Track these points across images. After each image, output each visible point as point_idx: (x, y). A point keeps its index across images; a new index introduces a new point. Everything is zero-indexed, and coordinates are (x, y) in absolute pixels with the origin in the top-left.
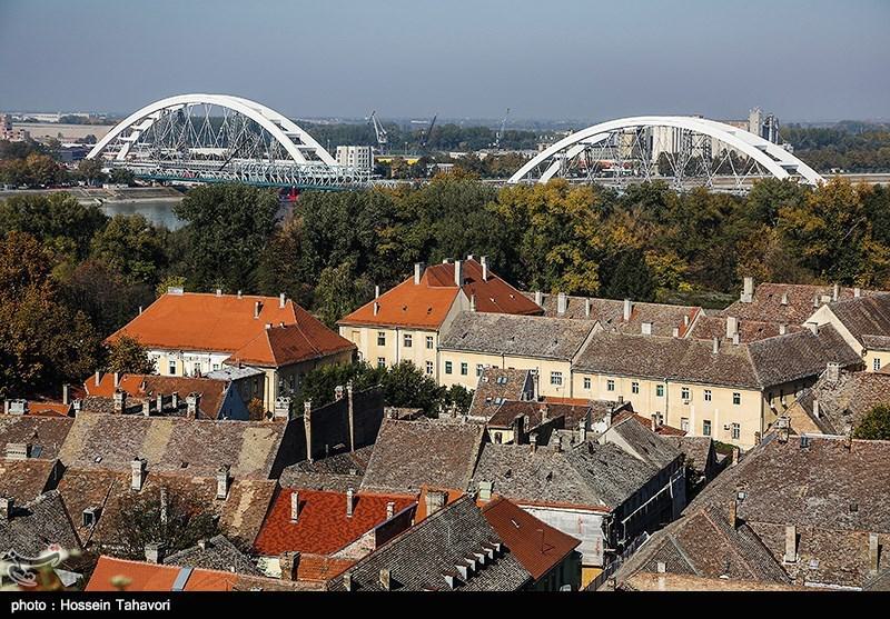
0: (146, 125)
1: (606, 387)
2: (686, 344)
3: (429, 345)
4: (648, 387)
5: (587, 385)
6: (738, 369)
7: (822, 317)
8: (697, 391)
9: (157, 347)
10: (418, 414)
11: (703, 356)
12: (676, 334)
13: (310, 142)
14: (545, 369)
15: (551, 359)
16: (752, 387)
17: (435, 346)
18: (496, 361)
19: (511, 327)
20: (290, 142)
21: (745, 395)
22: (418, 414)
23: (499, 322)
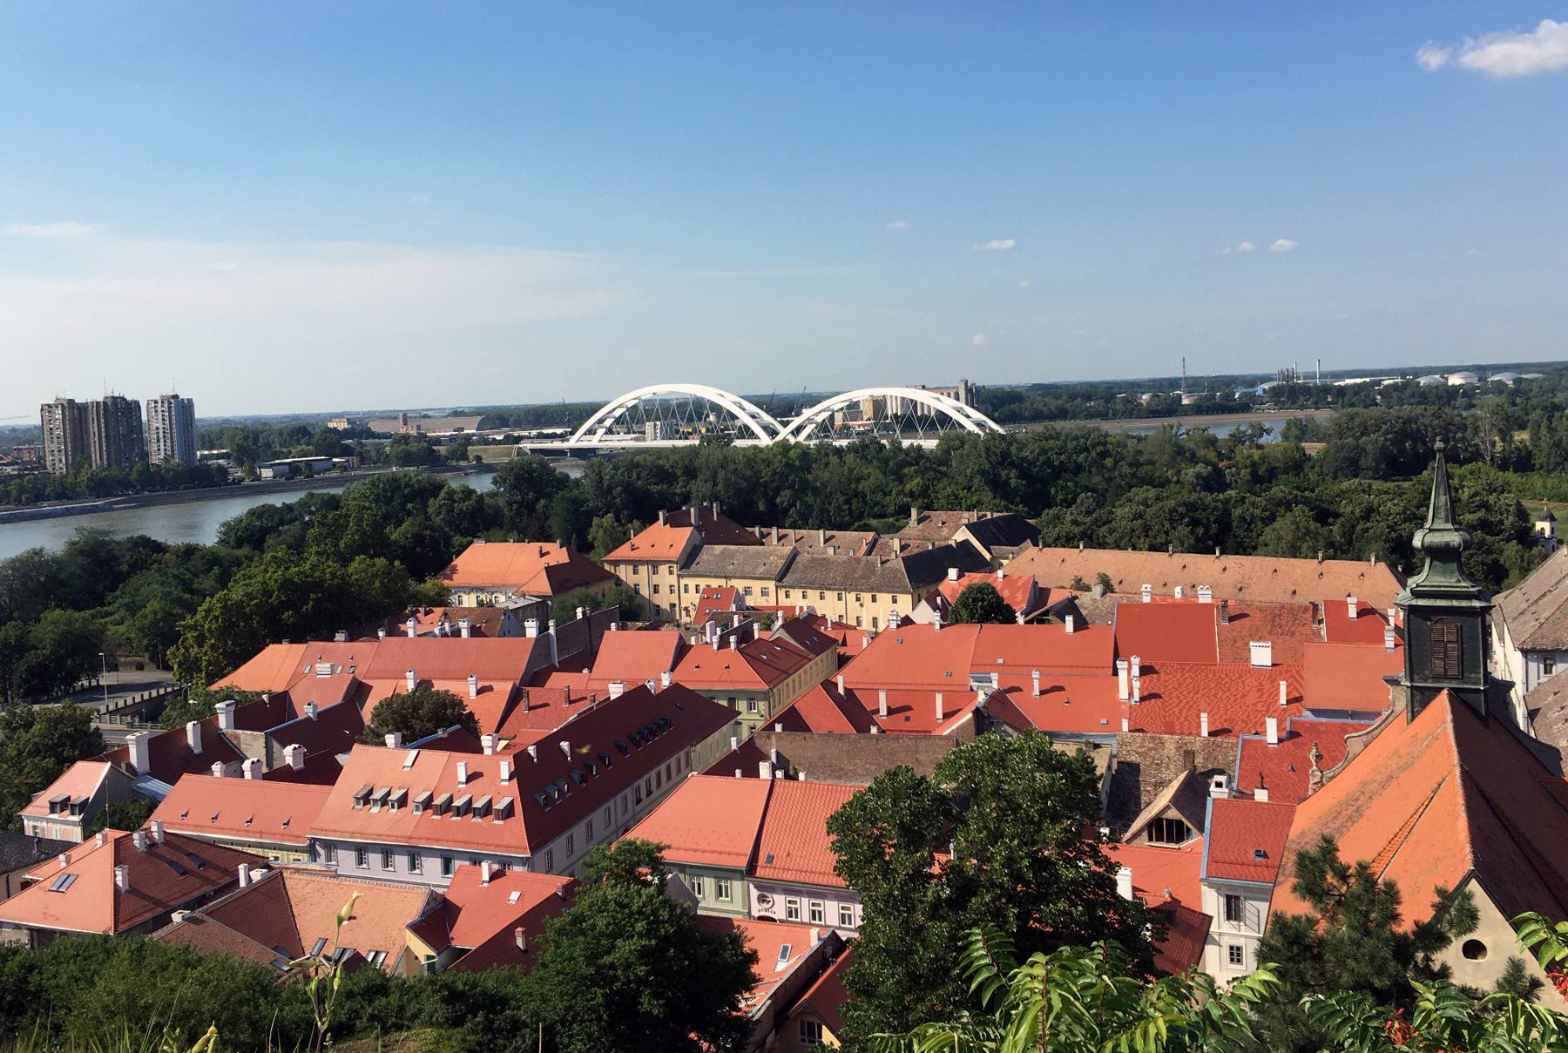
0: (617, 413)
1: (668, 573)
2: (858, 561)
3: (671, 573)
4: (831, 596)
5: (787, 596)
6: (895, 577)
7: (963, 535)
8: (867, 597)
9: (435, 679)
10: (1205, 988)
11: (871, 569)
12: (851, 554)
13: (767, 418)
14: (756, 586)
15: (760, 579)
16: (905, 592)
17: (675, 572)
18: (715, 583)
19: (732, 555)
20: (750, 419)
21: (900, 597)
22: (1205, 988)
23: (723, 552)
